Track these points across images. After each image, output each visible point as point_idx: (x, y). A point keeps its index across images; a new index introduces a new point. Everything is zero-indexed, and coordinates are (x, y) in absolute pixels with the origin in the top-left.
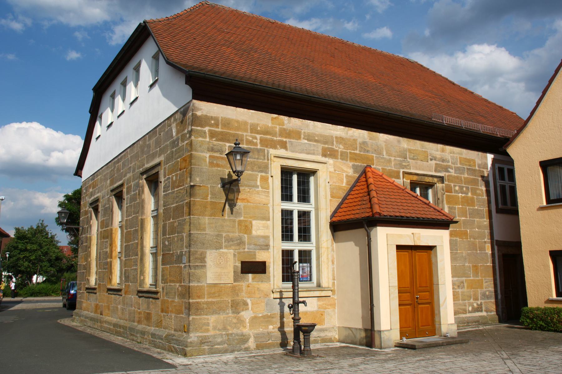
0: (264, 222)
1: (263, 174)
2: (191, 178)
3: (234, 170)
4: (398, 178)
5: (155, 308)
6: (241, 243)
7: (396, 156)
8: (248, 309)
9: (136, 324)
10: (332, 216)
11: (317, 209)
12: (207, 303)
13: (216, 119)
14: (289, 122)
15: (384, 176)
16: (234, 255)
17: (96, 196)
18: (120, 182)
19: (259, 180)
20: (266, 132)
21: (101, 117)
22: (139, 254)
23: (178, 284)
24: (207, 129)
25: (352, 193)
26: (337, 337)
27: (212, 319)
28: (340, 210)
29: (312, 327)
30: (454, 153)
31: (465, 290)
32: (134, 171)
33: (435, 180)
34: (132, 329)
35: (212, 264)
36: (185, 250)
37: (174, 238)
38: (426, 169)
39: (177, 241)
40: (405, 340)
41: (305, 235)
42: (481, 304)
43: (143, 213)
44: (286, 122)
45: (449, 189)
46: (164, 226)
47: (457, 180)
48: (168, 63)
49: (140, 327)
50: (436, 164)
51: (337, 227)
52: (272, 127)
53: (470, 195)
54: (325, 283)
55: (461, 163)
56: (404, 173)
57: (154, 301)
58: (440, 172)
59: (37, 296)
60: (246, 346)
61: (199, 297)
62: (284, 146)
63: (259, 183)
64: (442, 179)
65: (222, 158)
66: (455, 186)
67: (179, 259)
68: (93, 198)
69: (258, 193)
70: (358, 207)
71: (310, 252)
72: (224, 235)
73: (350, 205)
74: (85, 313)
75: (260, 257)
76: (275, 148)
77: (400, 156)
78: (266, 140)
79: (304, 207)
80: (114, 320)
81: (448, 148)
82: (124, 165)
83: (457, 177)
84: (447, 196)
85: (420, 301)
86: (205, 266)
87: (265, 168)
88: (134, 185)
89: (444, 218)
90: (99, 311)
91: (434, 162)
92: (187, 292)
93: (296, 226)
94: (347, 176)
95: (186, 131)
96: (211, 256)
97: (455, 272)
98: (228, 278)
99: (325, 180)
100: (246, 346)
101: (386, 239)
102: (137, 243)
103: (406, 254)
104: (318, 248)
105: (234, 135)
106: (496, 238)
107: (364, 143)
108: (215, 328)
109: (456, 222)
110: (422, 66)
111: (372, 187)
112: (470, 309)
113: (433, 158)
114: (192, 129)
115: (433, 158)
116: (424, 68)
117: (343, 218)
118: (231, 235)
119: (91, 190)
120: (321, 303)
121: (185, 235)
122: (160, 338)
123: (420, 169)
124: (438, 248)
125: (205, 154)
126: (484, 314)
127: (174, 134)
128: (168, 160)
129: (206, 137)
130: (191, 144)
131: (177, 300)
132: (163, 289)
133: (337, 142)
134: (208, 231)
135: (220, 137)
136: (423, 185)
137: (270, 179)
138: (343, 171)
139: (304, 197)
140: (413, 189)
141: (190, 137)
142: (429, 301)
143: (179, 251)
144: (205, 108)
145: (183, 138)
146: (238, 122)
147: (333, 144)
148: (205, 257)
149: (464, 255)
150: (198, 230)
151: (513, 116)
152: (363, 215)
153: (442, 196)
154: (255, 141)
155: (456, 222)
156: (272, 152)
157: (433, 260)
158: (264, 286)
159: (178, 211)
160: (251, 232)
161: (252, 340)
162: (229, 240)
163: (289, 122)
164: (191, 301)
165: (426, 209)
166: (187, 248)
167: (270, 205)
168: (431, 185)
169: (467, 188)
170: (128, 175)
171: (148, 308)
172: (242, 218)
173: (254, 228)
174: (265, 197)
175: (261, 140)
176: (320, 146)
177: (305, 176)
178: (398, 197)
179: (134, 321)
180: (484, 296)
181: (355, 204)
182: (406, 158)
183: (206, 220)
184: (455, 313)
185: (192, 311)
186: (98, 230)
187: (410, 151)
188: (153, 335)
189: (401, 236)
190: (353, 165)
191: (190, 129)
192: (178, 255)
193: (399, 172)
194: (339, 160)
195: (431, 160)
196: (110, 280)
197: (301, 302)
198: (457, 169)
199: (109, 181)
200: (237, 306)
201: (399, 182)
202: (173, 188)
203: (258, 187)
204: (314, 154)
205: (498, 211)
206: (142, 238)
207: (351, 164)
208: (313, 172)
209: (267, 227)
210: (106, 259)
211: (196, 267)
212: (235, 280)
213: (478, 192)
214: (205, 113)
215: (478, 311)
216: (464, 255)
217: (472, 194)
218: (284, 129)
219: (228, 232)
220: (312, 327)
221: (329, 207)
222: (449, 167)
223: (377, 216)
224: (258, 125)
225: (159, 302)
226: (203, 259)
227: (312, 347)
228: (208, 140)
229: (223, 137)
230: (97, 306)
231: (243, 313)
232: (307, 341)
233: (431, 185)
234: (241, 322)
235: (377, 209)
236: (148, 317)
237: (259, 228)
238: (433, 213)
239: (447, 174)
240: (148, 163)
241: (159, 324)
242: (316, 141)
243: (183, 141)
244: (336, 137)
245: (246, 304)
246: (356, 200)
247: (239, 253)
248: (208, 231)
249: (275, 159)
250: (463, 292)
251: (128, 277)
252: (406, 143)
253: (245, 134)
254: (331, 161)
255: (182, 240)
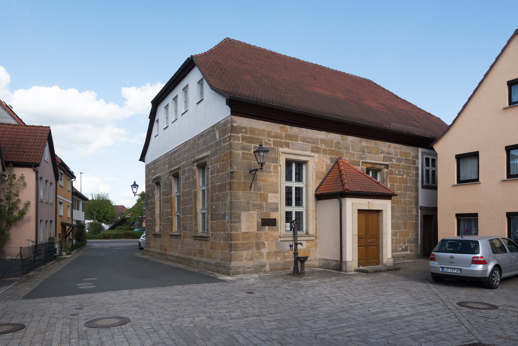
0: (275, 194)
1: (275, 164)
2: (231, 167)
3: (259, 162)
4: (359, 166)
5: (206, 247)
6: (261, 207)
7: (358, 151)
8: (265, 247)
9: (192, 256)
10: (316, 191)
11: (307, 186)
12: (242, 244)
13: (246, 128)
14: (291, 130)
15: (350, 165)
16: (258, 215)
17: (157, 175)
18: (177, 167)
19: (272, 168)
20: (277, 137)
21: (158, 121)
22: (194, 213)
23: (223, 233)
24: (240, 135)
25: (329, 175)
26: (317, 264)
27: (245, 253)
28: (321, 187)
29: (306, 258)
30: (396, 148)
31: (398, 237)
32: (187, 160)
33: (383, 167)
34: (190, 260)
35: (244, 220)
36: (228, 211)
37: (219, 204)
38: (377, 159)
39: (222, 206)
40: (361, 268)
41: (299, 202)
42: (407, 246)
43: (196, 188)
44: (289, 130)
45: (391, 173)
46: (212, 197)
47: (398, 166)
48: (212, 87)
49: (195, 258)
50: (384, 156)
51: (319, 197)
52: (280, 133)
53: (405, 176)
54: (311, 231)
55: (400, 156)
56: (363, 162)
57: (205, 242)
58: (386, 161)
59: (107, 239)
60: (264, 269)
61: (237, 240)
62: (287, 145)
63: (272, 170)
64: (387, 166)
65: (250, 154)
66: (395, 171)
67: (223, 217)
68: (155, 176)
69: (272, 176)
70: (334, 185)
71: (302, 212)
72: (251, 202)
73: (328, 183)
74: (153, 250)
75: (273, 215)
76: (282, 147)
77: (360, 151)
78: (277, 141)
79: (299, 185)
80: (176, 254)
81: (393, 145)
82: (179, 155)
83: (397, 165)
84: (390, 177)
85: (371, 244)
86: (240, 222)
87: (276, 160)
88: (188, 169)
89: (388, 192)
90: (164, 249)
91: (382, 155)
92: (229, 237)
93: (294, 197)
94: (326, 164)
95: (226, 136)
96: (244, 216)
97: (394, 226)
98: (254, 229)
99: (313, 167)
100: (264, 269)
101: (352, 206)
102: (192, 207)
103: (363, 215)
104: (307, 211)
105: (257, 139)
106: (420, 204)
107: (338, 143)
108: (246, 259)
109: (397, 195)
110: (375, 84)
111: (343, 172)
112: (400, 249)
113: (383, 152)
114: (231, 136)
115: (383, 152)
116: (377, 85)
117: (324, 192)
118: (255, 202)
119: (153, 171)
120: (309, 244)
121: (227, 203)
122: (211, 264)
123: (373, 160)
124: (384, 212)
125: (239, 152)
126: (409, 252)
127: (217, 138)
128: (213, 154)
129: (239, 141)
130: (231, 145)
131: (222, 242)
132: (212, 235)
133: (321, 142)
134: (242, 200)
135: (248, 140)
136: (375, 170)
137: (279, 167)
138: (324, 161)
139: (299, 178)
140: (368, 172)
141: (230, 140)
142: (376, 244)
143: (223, 213)
144: (241, 121)
145: (224, 141)
146: (259, 130)
147: (318, 144)
148: (240, 216)
149: (398, 215)
150: (236, 199)
151: (438, 121)
152: (337, 191)
153: (387, 178)
154: (270, 142)
155: (397, 195)
156: (281, 149)
157: (380, 219)
158: (275, 234)
159: (222, 188)
160: (267, 201)
161: (267, 266)
162: (254, 205)
163: (291, 130)
164: (232, 242)
165: (378, 187)
166: (228, 210)
167: (279, 184)
168: (380, 170)
169: (404, 172)
170: (183, 163)
171: (201, 246)
172: (262, 192)
173: (269, 198)
174: (277, 179)
175: (274, 142)
176: (310, 145)
177: (300, 164)
178: (359, 179)
179: (191, 255)
180: (409, 241)
181: (331, 183)
182: (364, 152)
183: (240, 193)
184: (392, 252)
185: (233, 249)
186: (160, 197)
187: (367, 147)
188: (206, 263)
189: (361, 204)
190: (331, 158)
191: (229, 135)
192: (223, 216)
193: (359, 162)
194: (322, 155)
195: (381, 153)
196: (172, 229)
197: (299, 244)
198: (398, 160)
199: (167, 166)
200: (259, 246)
201: (359, 168)
202: (218, 173)
203: (271, 172)
204: (306, 151)
205: (423, 187)
206: (195, 203)
207: (329, 157)
208: (306, 162)
209: (277, 198)
210: (168, 216)
211: (235, 222)
212: (258, 230)
213: (411, 174)
214: (239, 125)
215: (405, 251)
216: (398, 215)
217: (406, 176)
218: (288, 135)
219: (254, 200)
220: (306, 258)
221: (314, 185)
222: (393, 158)
223: (347, 191)
224: (271, 132)
225: (209, 243)
226: (239, 217)
227: (306, 270)
228: (241, 142)
229: (251, 140)
230: (162, 245)
231: (262, 250)
232: (303, 267)
233: (380, 170)
234: (261, 255)
235: (347, 187)
236: (201, 252)
237: (272, 198)
238: (381, 189)
239: (391, 163)
240: (198, 155)
241: (209, 256)
242: (308, 142)
243: (224, 142)
244: (320, 139)
245: (264, 244)
246: (332, 180)
247: (260, 213)
248: (242, 200)
249: (282, 154)
250: (396, 239)
251: (186, 227)
252: (365, 143)
253: (263, 138)
254: (317, 155)
255: (225, 205)
